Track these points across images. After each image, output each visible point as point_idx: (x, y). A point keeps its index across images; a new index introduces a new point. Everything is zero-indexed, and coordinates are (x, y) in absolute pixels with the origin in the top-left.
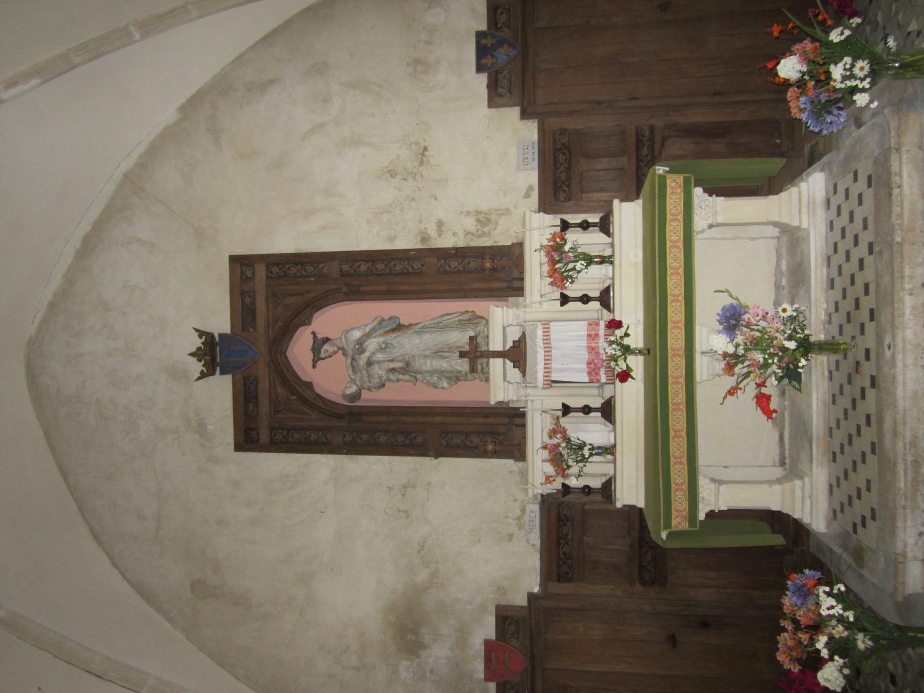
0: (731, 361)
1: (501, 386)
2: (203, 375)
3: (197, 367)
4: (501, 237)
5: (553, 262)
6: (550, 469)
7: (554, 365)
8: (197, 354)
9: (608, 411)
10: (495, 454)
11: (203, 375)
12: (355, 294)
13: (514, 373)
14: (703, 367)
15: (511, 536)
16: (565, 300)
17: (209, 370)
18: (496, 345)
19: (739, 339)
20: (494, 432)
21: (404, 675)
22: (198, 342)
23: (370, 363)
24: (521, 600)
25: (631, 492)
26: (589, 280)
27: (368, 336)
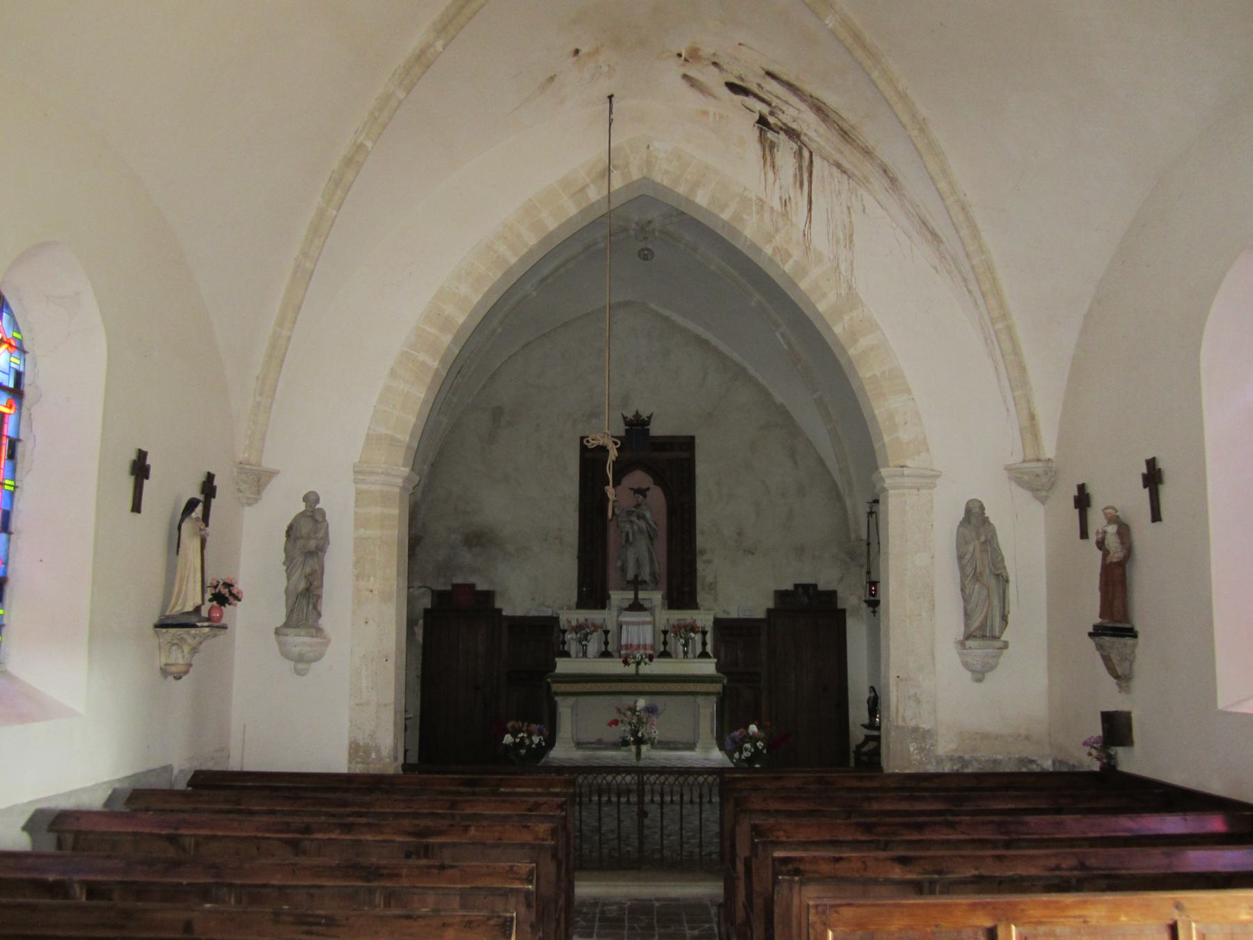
0: (633, 710)
1: (618, 597)
2: (625, 418)
3: (630, 415)
4: (701, 597)
5: (685, 627)
6: (574, 623)
7: (630, 627)
8: (637, 414)
9: (605, 654)
10: (580, 593)
11: (625, 418)
12: (671, 512)
13: (626, 605)
14: (628, 701)
15: (533, 599)
16: (665, 632)
17: (627, 422)
18: (642, 595)
19: (643, 714)
20: (592, 592)
21: (453, 536)
22: (645, 415)
23: (631, 522)
24: (498, 605)
25: (563, 666)
26: (677, 645)
27: (647, 523)
